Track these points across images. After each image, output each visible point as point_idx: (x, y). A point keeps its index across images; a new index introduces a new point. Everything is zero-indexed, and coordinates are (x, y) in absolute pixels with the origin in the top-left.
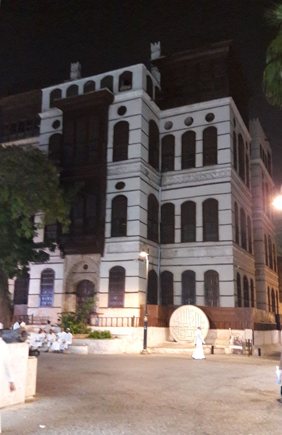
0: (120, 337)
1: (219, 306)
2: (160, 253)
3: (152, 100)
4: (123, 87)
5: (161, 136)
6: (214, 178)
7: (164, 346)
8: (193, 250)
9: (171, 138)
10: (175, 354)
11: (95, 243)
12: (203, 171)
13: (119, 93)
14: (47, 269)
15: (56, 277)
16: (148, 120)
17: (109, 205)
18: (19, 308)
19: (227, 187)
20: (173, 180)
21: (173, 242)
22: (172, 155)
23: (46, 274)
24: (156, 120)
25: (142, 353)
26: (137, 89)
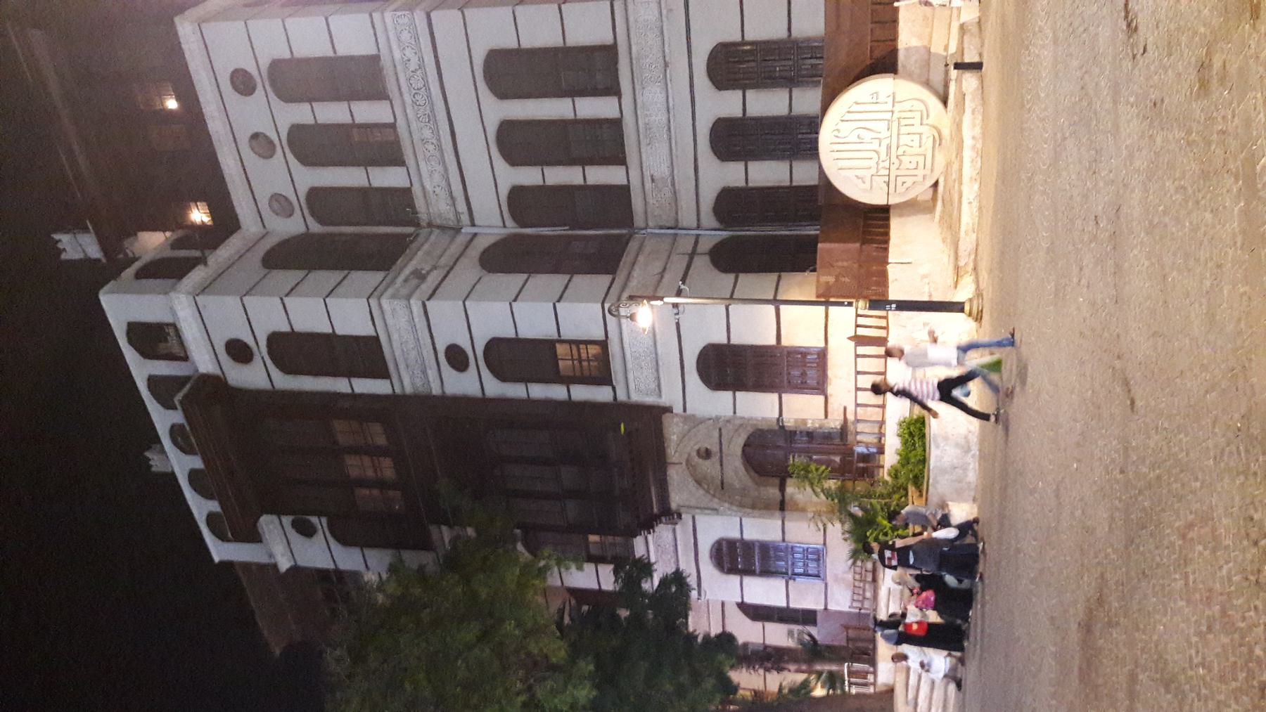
1: (823, 40)
2: (661, 228)
3: (202, 261)
5: (316, 227)
6: (422, 66)
7: (951, 225)
8: (648, 127)
9: (319, 200)
10: (979, 197)
14: (711, 557)
15: (735, 534)
17: (515, 391)
20: (437, 190)
21: (623, 192)
22: (365, 193)
23: (726, 559)
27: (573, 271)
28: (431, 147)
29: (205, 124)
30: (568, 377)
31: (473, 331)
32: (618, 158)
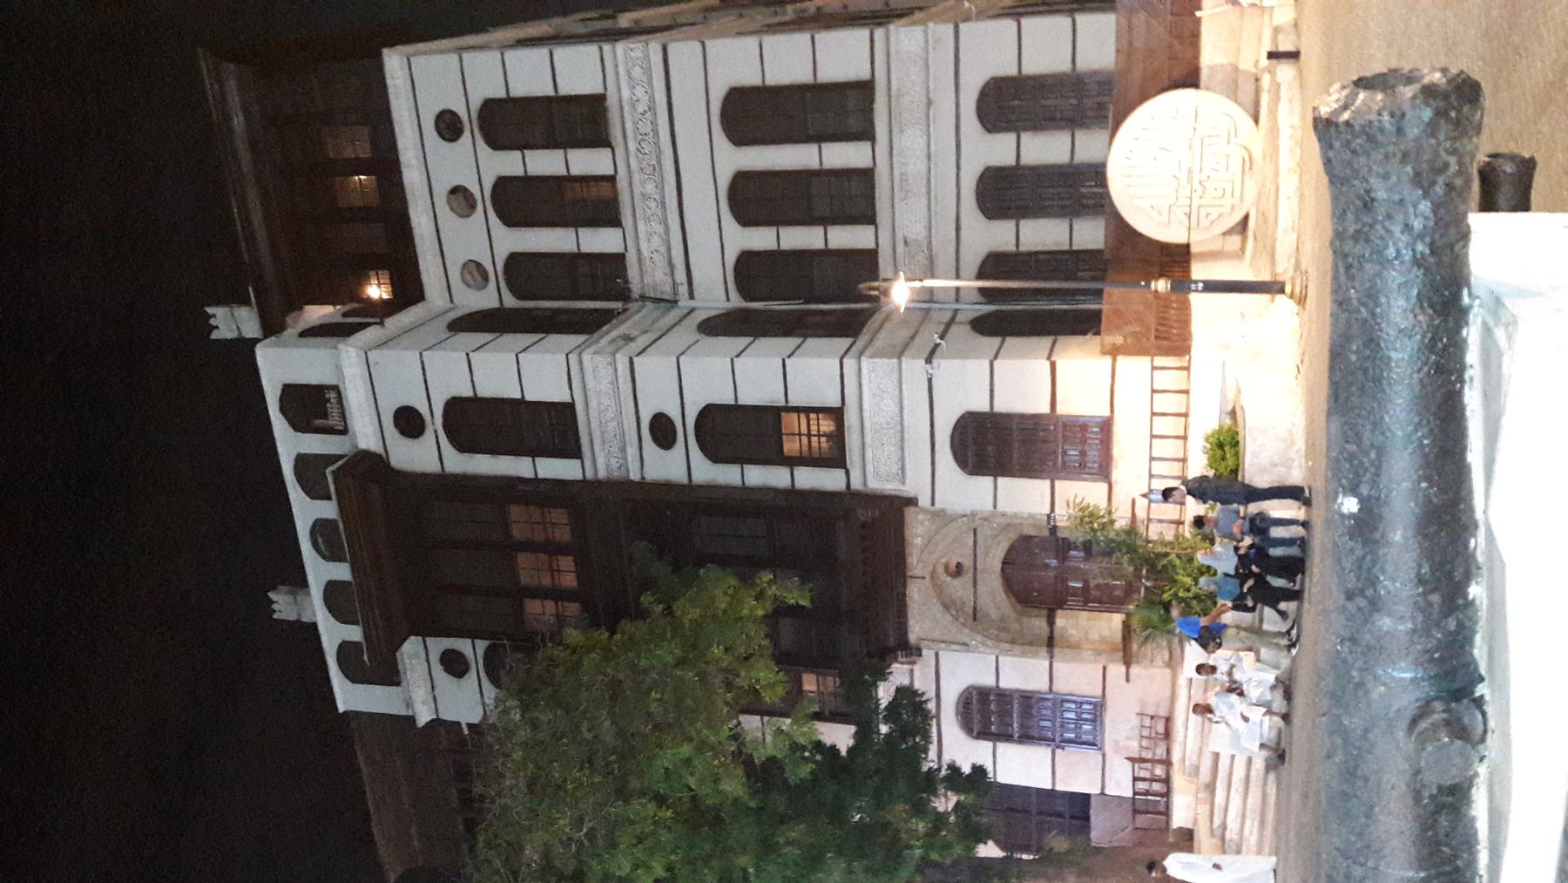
0: (1231, 395)
4: (334, 421)
5: (510, 301)
6: (652, 108)
9: (520, 269)
11: (863, 526)
12: (627, 148)
13: (351, 433)
15: (988, 680)
16: (448, 335)
17: (728, 475)
18: (1102, 828)
19: (684, 52)
20: (655, 256)
23: (977, 717)
24: (452, 316)
25: (1301, 301)
26: (338, 368)
27: (805, 336)
28: (653, 204)
29: (399, 172)
30: (794, 458)
31: (685, 396)
32: (867, 217)
